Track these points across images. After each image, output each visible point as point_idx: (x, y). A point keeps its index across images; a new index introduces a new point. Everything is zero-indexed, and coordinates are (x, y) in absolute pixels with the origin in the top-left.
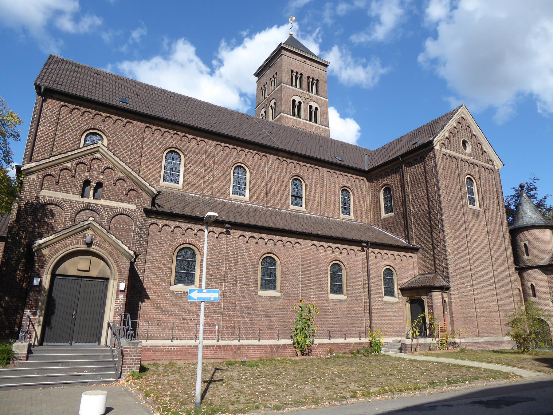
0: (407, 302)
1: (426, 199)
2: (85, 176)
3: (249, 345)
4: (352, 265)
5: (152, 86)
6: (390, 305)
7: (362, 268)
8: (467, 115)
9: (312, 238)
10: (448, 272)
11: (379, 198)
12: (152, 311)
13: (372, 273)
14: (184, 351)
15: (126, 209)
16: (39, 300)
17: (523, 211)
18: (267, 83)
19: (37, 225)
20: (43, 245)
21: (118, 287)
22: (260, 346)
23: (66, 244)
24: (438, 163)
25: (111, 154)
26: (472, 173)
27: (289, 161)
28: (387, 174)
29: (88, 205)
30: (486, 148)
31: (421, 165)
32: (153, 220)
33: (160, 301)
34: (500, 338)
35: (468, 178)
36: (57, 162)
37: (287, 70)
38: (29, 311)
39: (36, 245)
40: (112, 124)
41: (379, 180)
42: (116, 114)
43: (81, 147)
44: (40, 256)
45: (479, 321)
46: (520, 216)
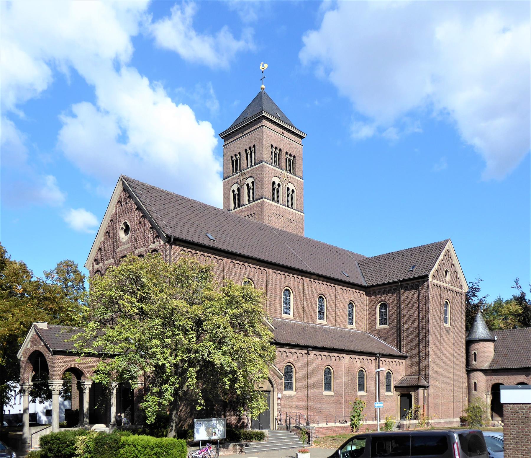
1: (417, 320)
5: (200, 202)
8: (451, 248)
11: (376, 311)
17: (477, 327)
24: (430, 293)
26: (449, 298)
28: (385, 293)
30: (460, 275)
34: (452, 420)
42: (213, 253)
45: (442, 408)
46: (474, 330)
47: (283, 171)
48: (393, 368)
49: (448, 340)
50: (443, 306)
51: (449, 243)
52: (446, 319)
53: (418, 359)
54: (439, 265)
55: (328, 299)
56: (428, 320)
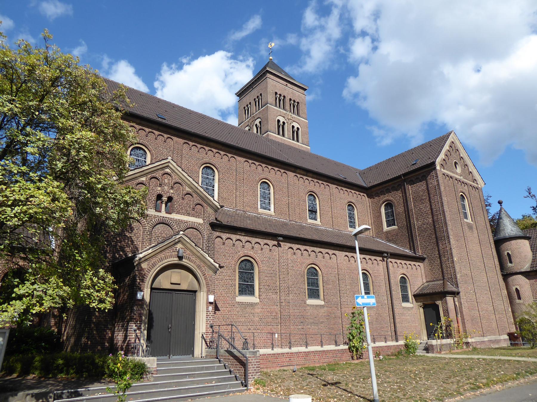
0: (421, 307)
1: (430, 214)
6: (407, 310)
11: (381, 212)
13: (392, 281)
14: (266, 359)
15: (195, 222)
17: (504, 224)
19: (118, 239)
20: (143, 259)
21: (208, 299)
22: (324, 351)
23: (161, 258)
25: (180, 170)
26: (464, 191)
27: (305, 177)
28: (388, 191)
32: (218, 234)
33: (228, 313)
34: (498, 337)
35: (461, 195)
36: (134, 176)
38: (134, 325)
39: (137, 259)
43: (148, 163)
46: (502, 228)
48: (408, 272)
50: (459, 199)
51: (453, 136)
54: (446, 155)
55: (320, 197)
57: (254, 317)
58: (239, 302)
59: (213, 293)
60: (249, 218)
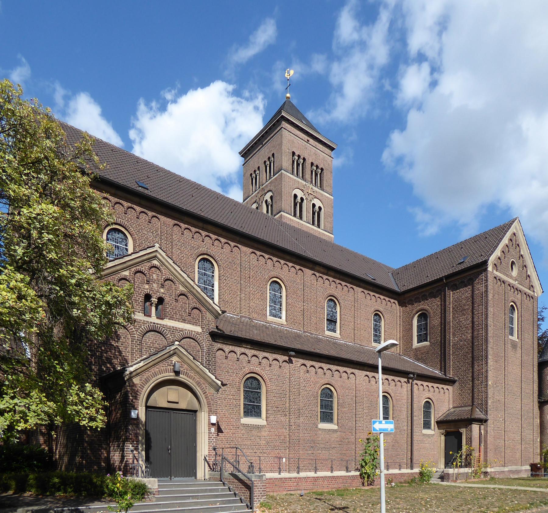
0: (442, 434)
1: (470, 328)
2: (145, 289)
3: (325, 477)
4: (398, 398)
6: (427, 438)
7: (406, 401)
9: (366, 368)
10: (487, 405)
11: (412, 325)
12: (226, 444)
13: (415, 406)
14: (272, 483)
15: (192, 331)
16: (139, 434)
18: (259, 168)
19: (103, 348)
20: (134, 374)
21: (209, 420)
23: (155, 372)
25: (171, 262)
26: (516, 300)
27: (325, 277)
28: (425, 298)
29: (153, 325)
30: (530, 272)
31: (469, 289)
32: (219, 346)
34: (519, 468)
35: (512, 306)
36: (114, 269)
37: (288, 151)
38: (131, 445)
40: (135, 217)
41: (413, 304)
44: (132, 386)
45: (506, 451)
47: (307, 183)
48: (434, 396)
49: (514, 357)
52: (512, 329)
53: (471, 383)
55: (342, 304)
56: (487, 326)
57: (260, 440)
58: (244, 424)
59: (216, 414)
60: (256, 327)
